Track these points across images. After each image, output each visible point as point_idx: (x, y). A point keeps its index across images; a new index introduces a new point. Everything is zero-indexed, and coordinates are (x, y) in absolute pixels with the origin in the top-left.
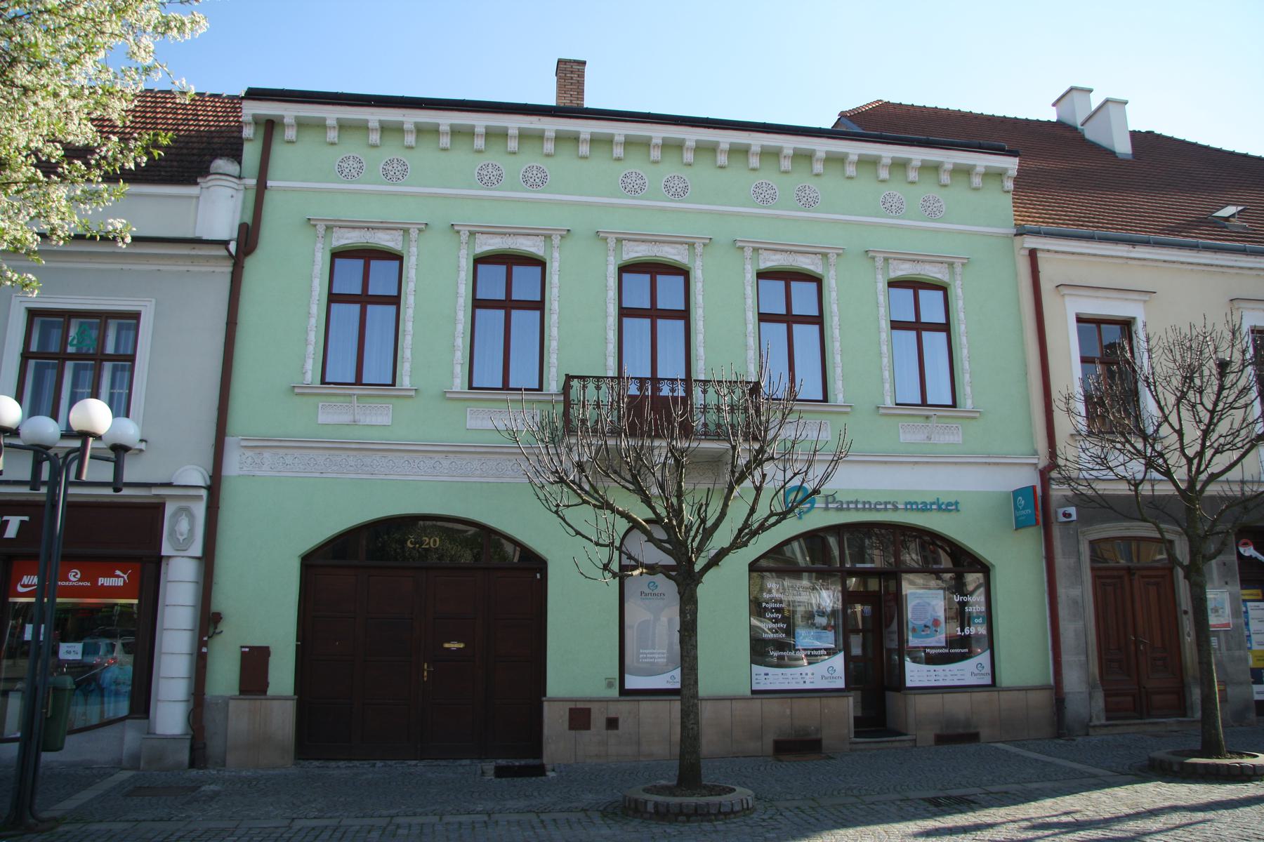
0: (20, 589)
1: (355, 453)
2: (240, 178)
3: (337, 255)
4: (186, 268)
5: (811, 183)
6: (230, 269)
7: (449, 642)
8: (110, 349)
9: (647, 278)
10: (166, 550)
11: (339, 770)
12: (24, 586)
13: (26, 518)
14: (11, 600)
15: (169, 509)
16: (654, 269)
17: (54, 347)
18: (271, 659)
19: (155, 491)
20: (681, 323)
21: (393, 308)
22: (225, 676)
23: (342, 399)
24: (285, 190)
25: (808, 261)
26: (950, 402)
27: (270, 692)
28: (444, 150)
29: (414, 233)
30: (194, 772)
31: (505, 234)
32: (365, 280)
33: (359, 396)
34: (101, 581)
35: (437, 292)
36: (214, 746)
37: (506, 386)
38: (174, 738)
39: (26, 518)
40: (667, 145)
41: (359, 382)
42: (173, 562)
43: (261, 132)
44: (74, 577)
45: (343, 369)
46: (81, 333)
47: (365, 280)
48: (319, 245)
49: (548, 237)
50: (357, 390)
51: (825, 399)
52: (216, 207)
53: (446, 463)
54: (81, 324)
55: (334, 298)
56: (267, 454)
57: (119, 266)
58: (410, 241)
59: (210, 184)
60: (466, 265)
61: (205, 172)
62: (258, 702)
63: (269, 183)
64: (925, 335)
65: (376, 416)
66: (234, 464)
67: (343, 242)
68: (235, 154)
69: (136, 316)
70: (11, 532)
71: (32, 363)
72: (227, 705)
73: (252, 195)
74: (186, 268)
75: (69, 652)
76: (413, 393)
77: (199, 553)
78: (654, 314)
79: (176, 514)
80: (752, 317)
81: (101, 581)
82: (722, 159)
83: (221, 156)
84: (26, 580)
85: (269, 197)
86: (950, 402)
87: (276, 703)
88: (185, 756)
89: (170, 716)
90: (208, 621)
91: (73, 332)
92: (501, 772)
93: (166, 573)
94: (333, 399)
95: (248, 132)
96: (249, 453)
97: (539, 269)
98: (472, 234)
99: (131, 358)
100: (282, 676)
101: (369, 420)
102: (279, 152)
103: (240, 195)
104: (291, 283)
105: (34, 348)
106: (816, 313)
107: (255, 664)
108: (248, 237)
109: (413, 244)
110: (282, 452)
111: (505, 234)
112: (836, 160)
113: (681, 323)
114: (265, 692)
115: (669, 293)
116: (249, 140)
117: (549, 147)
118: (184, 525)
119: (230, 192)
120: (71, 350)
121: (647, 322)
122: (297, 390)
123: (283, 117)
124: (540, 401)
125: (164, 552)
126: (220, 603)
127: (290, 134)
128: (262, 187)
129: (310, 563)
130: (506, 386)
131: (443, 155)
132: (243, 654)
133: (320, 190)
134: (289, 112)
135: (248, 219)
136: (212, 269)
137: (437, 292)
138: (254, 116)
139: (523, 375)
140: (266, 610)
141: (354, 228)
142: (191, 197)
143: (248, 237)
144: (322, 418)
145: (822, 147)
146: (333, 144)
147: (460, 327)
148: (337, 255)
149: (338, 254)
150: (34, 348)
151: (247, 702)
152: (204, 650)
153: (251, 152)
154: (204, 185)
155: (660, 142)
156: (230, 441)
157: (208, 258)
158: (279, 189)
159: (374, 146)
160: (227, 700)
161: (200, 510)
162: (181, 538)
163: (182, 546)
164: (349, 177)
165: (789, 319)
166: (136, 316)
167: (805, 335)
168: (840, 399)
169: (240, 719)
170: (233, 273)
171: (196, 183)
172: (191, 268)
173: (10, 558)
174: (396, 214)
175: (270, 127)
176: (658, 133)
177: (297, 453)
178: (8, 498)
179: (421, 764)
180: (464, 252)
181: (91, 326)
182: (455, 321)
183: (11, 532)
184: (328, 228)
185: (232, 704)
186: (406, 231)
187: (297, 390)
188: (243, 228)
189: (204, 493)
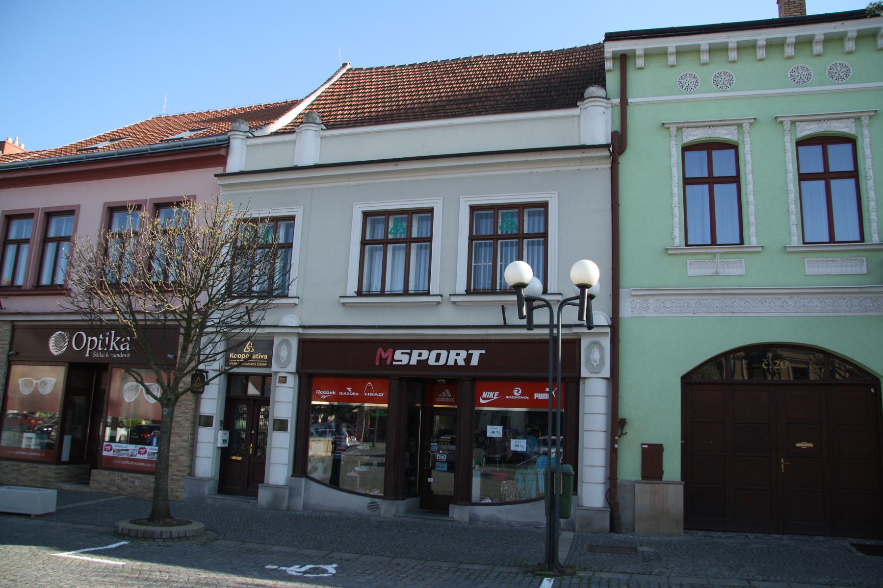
0: (482, 401)
1: (719, 297)
2: (607, 98)
3: (686, 148)
4: (576, 168)
5: (728, 68)
6: (610, 166)
7: (800, 442)
8: (415, 234)
9: (819, 148)
10: (584, 373)
11: (720, 538)
12: (484, 399)
13: (484, 352)
14: (476, 408)
15: (584, 343)
16: (710, 146)
17: (380, 236)
18: (664, 454)
19: (575, 330)
20: (734, 186)
21: (734, 186)
22: (631, 466)
23: (704, 256)
24: (641, 104)
25: (725, 132)
26: (858, 239)
27: (665, 478)
28: (761, 60)
29: (746, 127)
30: (616, 536)
31: (820, 120)
32: (711, 166)
33: (721, 253)
34: (536, 396)
35: (769, 171)
36: (625, 516)
37: (832, 240)
38: (598, 510)
39: (484, 352)
40: (713, 50)
41: (714, 243)
42: (588, 382)
43: (618, 64)
44: (517, 393)
45: (701, 234)
46: (396, 225)
47: (711, 166)
48: (673, 142)
49: (858, 119)
50: (715, 249)
51: (742, 242)
52: (593, 121)
53: (791, 302)
54: (395, 220)
55: (687, 181)
56: (651, 300)
57: (529, 171)
58: (743, 133)
59: (587, 105)
60: (676, 153)
61: (582, 98)
62: (657, 486)
63: (629, 101)
64: (833, 183)
65: (733, 269)
66: (627, 310)
67: (691, 138)
68: (602, 84)
69: (431, 210)
70: (169, 356)
71: (367, 247)
72: (634, 487)
73: (617, 110)
74: (576, 168)
75: (517, 446)
76: (760, 249)
77: (608, 376)
78: (711, 181)
79: (280, 344)
80: (792, 176)
81: (536, 396)
82: (761, 53)
83: (587, 87)
84: (485, 394)
85: (630, 110)
86: (858, 239)
87: (670, 487)
88: (607, 524)
89: (592, 493)
90: (617, 426)
91: (391, 225)
92: (860, 548)
93: (583, 390)
94: (698, 257)
95: (608, 65)
96: (637, 300)
97: (732, 151)
98: (793, 123)
99: (429, 240)
100: (672, 465)
101: (731, 271)
102: (633, 76)
103: (609, 111)
104: (655, 174)
105: (368, 238)
106: (851, 169)
107: (652, 456)
108: (618, 145)
109: (746, 135)
110: (663, 298)
111: (820, 120)
112: (774, 46)
113: (852, 182)
114: (661, 478)
115: (723, 165)
116: (609, 71)
117: (733, 55)
118: (596, 355)
119: (603, 109)
120: (390, 236)
121: (706, 187)
122: (670, 252)
123: (634, 51)
124: (865, 251)
125: (583, 374)
126: (625, 411)
127: (640, 62)
128: (624, 103)
129: (688, 381)
130: (832, 240)
131: (760, 64)
132: (643, 449)
133: (666, 103)
134: (639, 46)
135: (617, 128)
136: (596, 167)
137: (769, 171)
138: (613, 52)
139: (846, 229)
140: (659, 418)
141: (698, 127)
142: (573, 116)
143: (618, 145)
144: (691, 272)
145: (762, 36)
146: (672, 66)
147: (676, 199)
148: (686, 148)
149: (801, 143)
150: (368, 238)
151: (648, 486)
152: (616, 446)
153: (612, 79)
154: (582, 107)
155: (674, 50)
156: (622, 292)
157: (593, 159)
158: (637, 104)
159: (705, 64)
160: (633, 484)
161: (606, 342)
162: (595, 364)
163: (595, 370)
164: (688, 90)
165: (827, 176)
166: (431, 210)
167: (842, 189)
168: (754, 241)
169: (644, 498)
170: (612, 168)
171: (576, 106)
172: (580, 167)
173: (474, 379)
174: (730, 112)
175: (623, 59)
176: (704, 41)
177: (673, 298)
178: (397, 338)
179: (785, 537)
180: (787, 138)
181: (402, 220)
182: (787, 191)
183: (169, 356)
184: (679, 129)
185: (637, 485)
186: (740, 126)
187: (670, 252)
188: (614, 134)
189: (608, 330)
